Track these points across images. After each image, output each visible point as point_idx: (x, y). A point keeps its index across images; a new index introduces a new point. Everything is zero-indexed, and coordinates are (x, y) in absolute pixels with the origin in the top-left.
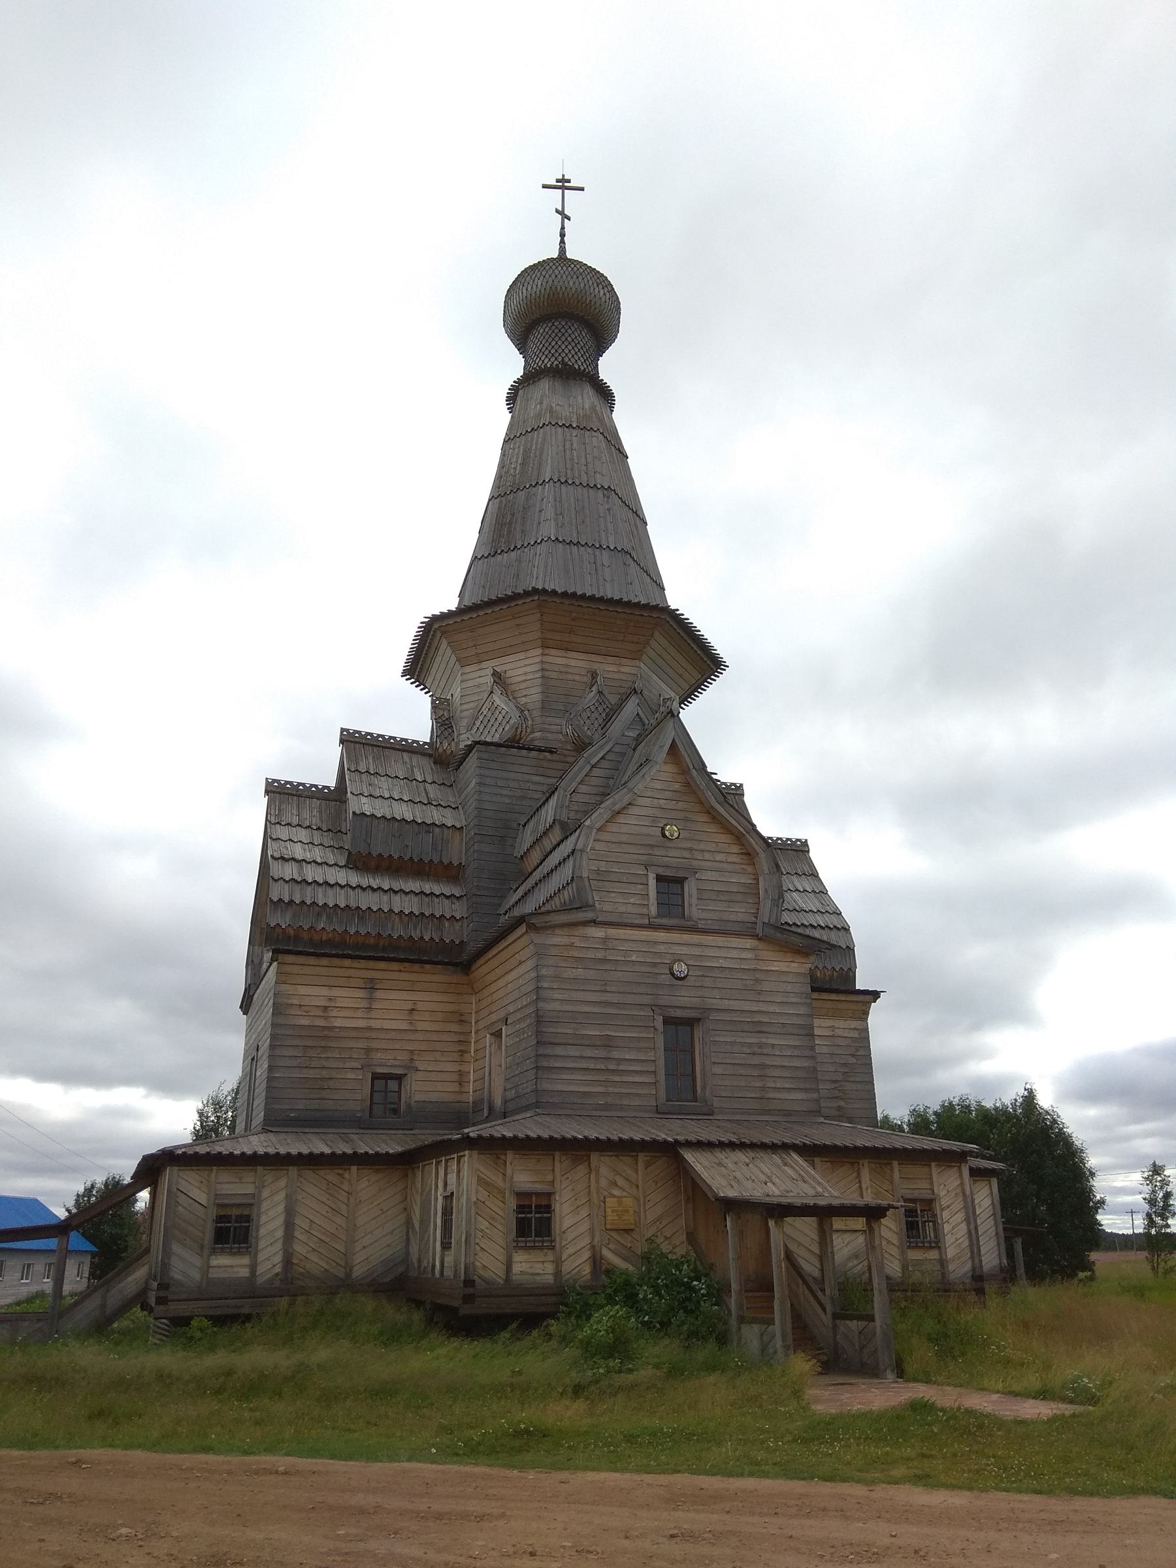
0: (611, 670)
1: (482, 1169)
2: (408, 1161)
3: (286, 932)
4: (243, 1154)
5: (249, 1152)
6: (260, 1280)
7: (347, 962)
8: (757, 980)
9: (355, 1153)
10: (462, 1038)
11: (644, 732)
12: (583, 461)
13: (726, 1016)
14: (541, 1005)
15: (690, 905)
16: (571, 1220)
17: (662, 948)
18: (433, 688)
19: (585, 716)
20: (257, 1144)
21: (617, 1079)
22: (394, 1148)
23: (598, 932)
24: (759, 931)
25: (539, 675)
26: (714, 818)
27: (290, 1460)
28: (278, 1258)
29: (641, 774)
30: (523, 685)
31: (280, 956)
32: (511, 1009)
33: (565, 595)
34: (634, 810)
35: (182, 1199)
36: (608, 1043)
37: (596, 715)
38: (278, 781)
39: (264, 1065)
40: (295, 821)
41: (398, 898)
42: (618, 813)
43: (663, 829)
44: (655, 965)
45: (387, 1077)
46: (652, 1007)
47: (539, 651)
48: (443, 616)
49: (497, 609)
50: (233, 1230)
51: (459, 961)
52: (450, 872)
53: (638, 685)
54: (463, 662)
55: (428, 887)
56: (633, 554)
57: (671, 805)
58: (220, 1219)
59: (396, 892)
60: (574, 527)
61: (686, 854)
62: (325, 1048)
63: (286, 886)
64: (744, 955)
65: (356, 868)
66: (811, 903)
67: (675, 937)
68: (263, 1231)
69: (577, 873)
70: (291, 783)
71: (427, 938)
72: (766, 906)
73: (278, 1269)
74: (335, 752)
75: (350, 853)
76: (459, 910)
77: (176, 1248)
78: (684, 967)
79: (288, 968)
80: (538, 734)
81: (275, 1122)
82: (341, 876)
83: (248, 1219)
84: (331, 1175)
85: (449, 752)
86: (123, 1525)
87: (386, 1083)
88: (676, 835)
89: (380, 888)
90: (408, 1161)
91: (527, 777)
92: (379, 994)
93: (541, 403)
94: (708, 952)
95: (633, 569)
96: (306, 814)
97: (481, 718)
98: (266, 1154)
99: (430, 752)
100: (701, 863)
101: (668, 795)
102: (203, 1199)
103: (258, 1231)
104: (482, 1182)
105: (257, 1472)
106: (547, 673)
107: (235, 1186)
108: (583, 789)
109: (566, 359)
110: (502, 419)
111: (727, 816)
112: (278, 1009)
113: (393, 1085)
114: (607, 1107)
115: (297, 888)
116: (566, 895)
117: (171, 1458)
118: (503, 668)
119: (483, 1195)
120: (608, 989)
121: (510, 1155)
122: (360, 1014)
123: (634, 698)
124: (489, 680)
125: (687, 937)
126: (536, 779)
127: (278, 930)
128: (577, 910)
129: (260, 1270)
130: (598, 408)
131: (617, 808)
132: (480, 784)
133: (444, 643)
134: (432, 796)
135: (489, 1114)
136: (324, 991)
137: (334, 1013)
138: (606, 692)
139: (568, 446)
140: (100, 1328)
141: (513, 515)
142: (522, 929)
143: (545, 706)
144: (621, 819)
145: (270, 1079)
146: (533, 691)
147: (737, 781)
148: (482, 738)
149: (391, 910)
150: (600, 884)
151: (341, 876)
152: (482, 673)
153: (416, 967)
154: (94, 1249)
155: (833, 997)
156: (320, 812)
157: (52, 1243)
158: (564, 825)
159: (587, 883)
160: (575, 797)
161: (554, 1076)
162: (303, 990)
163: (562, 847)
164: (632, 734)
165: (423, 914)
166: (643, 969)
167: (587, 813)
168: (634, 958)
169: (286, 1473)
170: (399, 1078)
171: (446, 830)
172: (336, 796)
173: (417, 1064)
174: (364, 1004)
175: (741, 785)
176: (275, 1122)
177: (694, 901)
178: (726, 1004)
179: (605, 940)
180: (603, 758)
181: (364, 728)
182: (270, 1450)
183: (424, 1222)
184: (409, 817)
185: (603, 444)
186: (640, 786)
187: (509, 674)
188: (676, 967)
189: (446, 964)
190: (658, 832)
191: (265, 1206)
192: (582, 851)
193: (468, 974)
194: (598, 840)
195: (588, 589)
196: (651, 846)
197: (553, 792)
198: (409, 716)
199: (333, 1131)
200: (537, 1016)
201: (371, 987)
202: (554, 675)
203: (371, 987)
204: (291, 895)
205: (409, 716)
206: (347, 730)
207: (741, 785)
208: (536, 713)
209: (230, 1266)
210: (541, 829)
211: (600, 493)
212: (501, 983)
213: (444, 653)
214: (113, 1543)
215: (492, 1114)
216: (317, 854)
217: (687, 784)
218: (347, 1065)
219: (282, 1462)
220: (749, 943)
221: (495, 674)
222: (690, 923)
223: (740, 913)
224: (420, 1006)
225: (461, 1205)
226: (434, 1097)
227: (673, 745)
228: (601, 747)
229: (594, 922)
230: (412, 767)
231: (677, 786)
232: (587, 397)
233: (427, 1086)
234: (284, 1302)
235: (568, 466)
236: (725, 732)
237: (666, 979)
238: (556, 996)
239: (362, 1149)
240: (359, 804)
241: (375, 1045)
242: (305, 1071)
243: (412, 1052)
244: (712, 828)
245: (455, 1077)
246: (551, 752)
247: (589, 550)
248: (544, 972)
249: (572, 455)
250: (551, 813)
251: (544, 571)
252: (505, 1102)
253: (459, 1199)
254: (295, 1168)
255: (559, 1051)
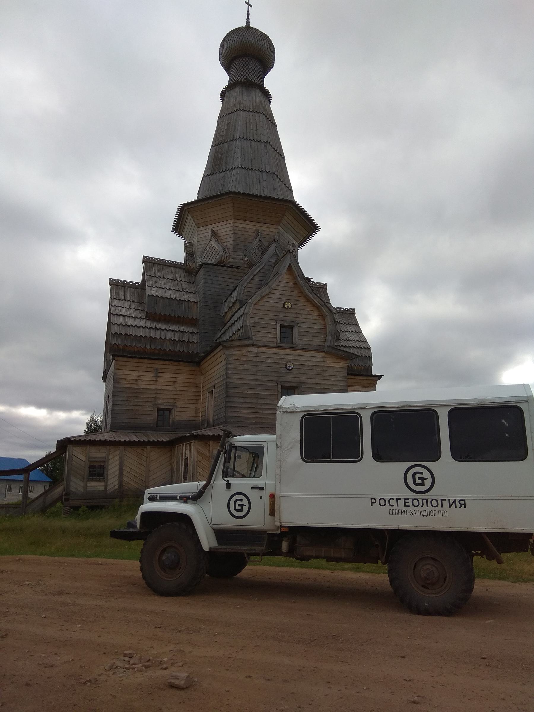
0: (266, 230)
1: (199, 448)
2: (171, 445)
3: (120, 348)
4: (100, 440)
5: (103, 440)
6: (109, 492)
7: (146, 361)
8: (323, 371)
9: (149, 441)
10: (197, 394)
11: (278, 260)
12: (255, 128)
13: (308, 386)
14: (228, 380)
15: (295, 338)
16: (113, 468)
17: (282, 357)
18: (186, 237)
19: (253, 252)
20: (107, 436)
21: (261, 412)
22: (165, 439)
23: (254, 350)
24: (325, 349)
25: (232, 232)
26: (307, 299)
27: (104, 560)
28: (116, 483)
29: (275, 279)
30: (225, 237)
31: (116, 358)
32: (216, 382)
33: (244, 194)
34: (271, 296)
35: (75, 458)
36: (257, 397)
37: (258, 251)
38: (115, 280)
39: (110, 404)
40: (123, 298)
41: (170, 333)
42: (264, 297)
43: (284, 304)
44: (278, 364)
45: (164, 410)
46: (277, 382)
47: (232, 221)
48: (189, 204)
49: (206, 202)
50: (97, 471)
51: (195, 361)
52: (193, 322)
53: (276, 238)
54: (198, 226)
55: (182, 329)
56: (278, 175)
57: (289, 293)
58: (91, 467)
59: (168, 331)
60: (250, 161)
61: (294, 315)
62: (137, 397)
63: (118, 327)
64: (319, 360)
65: (150, 319)
66: (354, 337)
67: (288, 352)
68: (110, 472)
69: (245, 323)
70: (121, 281)
71: (182, 351)
72: (329, 338)
73: (116, 487)
74: (140, 266)
75: (147, 313)
76: (196, 339)
77: (73, 479)
78: (291, 365)
79: (120, 363)
80: (232, 260)
81: (115, 427)
82: (143, 323)
83: (104, 467)
84: (139, 450)
85: (192, 267)
86: (28, 581)
87: (163, 413)
88: (290, 307)
89: (160, 329)
90: (171, 445)
91: (226, 279)
92: (160, 375)
93: (236, 99)
94: (302, 358)
95: (277, 182)
96: (128, 295)
97: (206, 252)
98: (110, 441)
99: (184, 267)
100: (301, 319)
101: (287, 289)
102: (84, 459)
103: (107, 471)
104: (199, 453)
105: (90, 564)
106: (236, 232)
107: (97, 453)
108: (250, 285)
109: (248, 77)
110: (218, 105)
111: (313, 298)
112: (116, 381)
113: (167, 413)
114: (256, 423)
115: (123, 328)
116: (240, 333)
117: (57, 558)
118: (217, 228)
119: (200, 458)
120: (258, 374)
121: (212, 443)
122: (151, 383)
123: (274, 244)
124: (210, 234)
125: (293, 352)
126: (230, 280)
127: (115, 346)
128: (245, 340)
129: (108, 488)
130: (263, 102)
131: (263, 295)
132: (205, 283)
133: (190, 217)
134: (184, 287)
135: (208, 426)
136: (136, 373)
137: (140, 382)
138: (263, 241)
139: (248, 121)
140: (43, 510)
141: (222, 155)
142: (220, 347)
143: (235, 247)
144: (265, 299)
145: (112, 410)
146: (229, 240)
147: (324, 282)
148: (207, 261)
149: (165, 338)
150: (255, 328)
151: (143, 323)
152: (207, 231)
153: (176, 363)
154: (51, 480)
155: (361, 378)
156: (134, 294)
157: (21, 477)
158: (241, 302)
159: (249, 328)
160: (247, 289)
161: (233, 410)
162: (127, 372)
163: (239, 312)
164: (273, 260)
165: (180, 340)
166: (273, 365)
167: (251, 297)
168: (269, 361)
169: (102, 564)
170: (170, 410)
171: (190, 303)
172: (141, 288)
173: (177, 404)
174: (154, 379)
175: (326, 284)
176: (115, 427)
177: (297, 335)
178: (309, 381)
179: (257, 353)
180: (259, 271)
181: (154, 256)
182: (98, 556)
183: (178, 469)
184: (173, 297)
185: (265, 120)
186: (274, 285)
187: (219, 232)
188: (288, 364)
189: (190, 362)
190: (282, 305)
191: (110, 462)
192: (247, 314)
193: (199, 367)
194: (255, 309)
195: (255, 191)
196: (279, 312)
197: (236, 287)
198: (173, 250)
199: (140, 432)
200: (227, 385)
201: (156, 371)
202: (239, 232)
203: (156, 371)
204: (121, 331)
205: (173, 250)
206: (146, 257)
207: (326, 284)
208: (231, 250)
209: (96, 486)
210: (231, 303)
211: (263, 145)
212: (213, 371)
213: (190, 222)
214: (21, 587)
215: (209, 425)
216: (133, 313)
217: (296, 284)
218: (146, 404)
219: (100, 560)
220: (321, 354)
221: (213, 231)
222: (295, 346)
223: (317, 341)
224: (178, 380)
225: (191, 462)
226: (184, 418)
227: (290, 266)
228: (259, 266)
229: (252, 345)
230: (175, 274)
231: (291, 285)
232: (258, 96)
233: (182, 413)
234: (117, 500)
235: (248, 131)
236: (313, 259)
237: (283, 370)
238: (235, 377)
239: (153, 439)
240: (151, 291)
241: (159, 396)
242: (128, 407)
243: (175, 399)
244: (306, 304)
245: (194, 410)
246: (238, 268)
247: (257, 173)
248: (229, 366)
249: (250, 126)
250: (235, 296)
251: (236, 183)
252: (214, 421)
253: (190, 460)
254: (123, 447)
255: (236, 400)
